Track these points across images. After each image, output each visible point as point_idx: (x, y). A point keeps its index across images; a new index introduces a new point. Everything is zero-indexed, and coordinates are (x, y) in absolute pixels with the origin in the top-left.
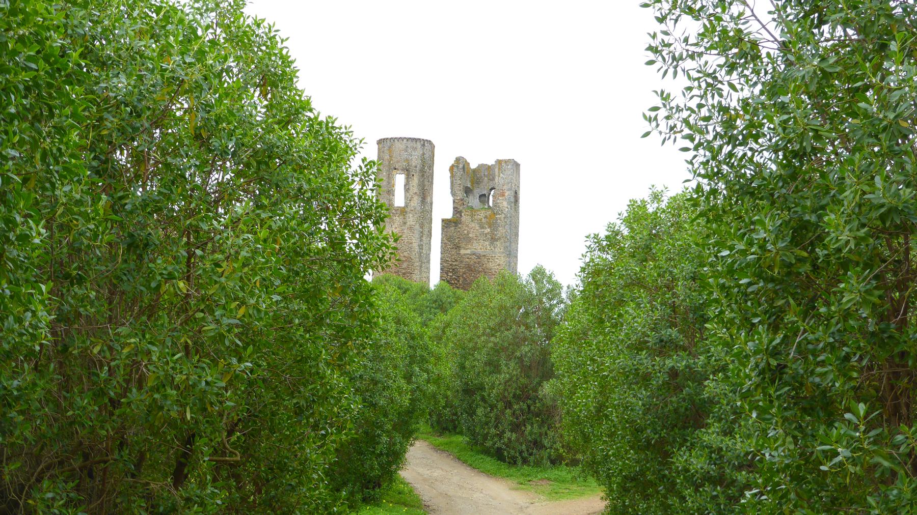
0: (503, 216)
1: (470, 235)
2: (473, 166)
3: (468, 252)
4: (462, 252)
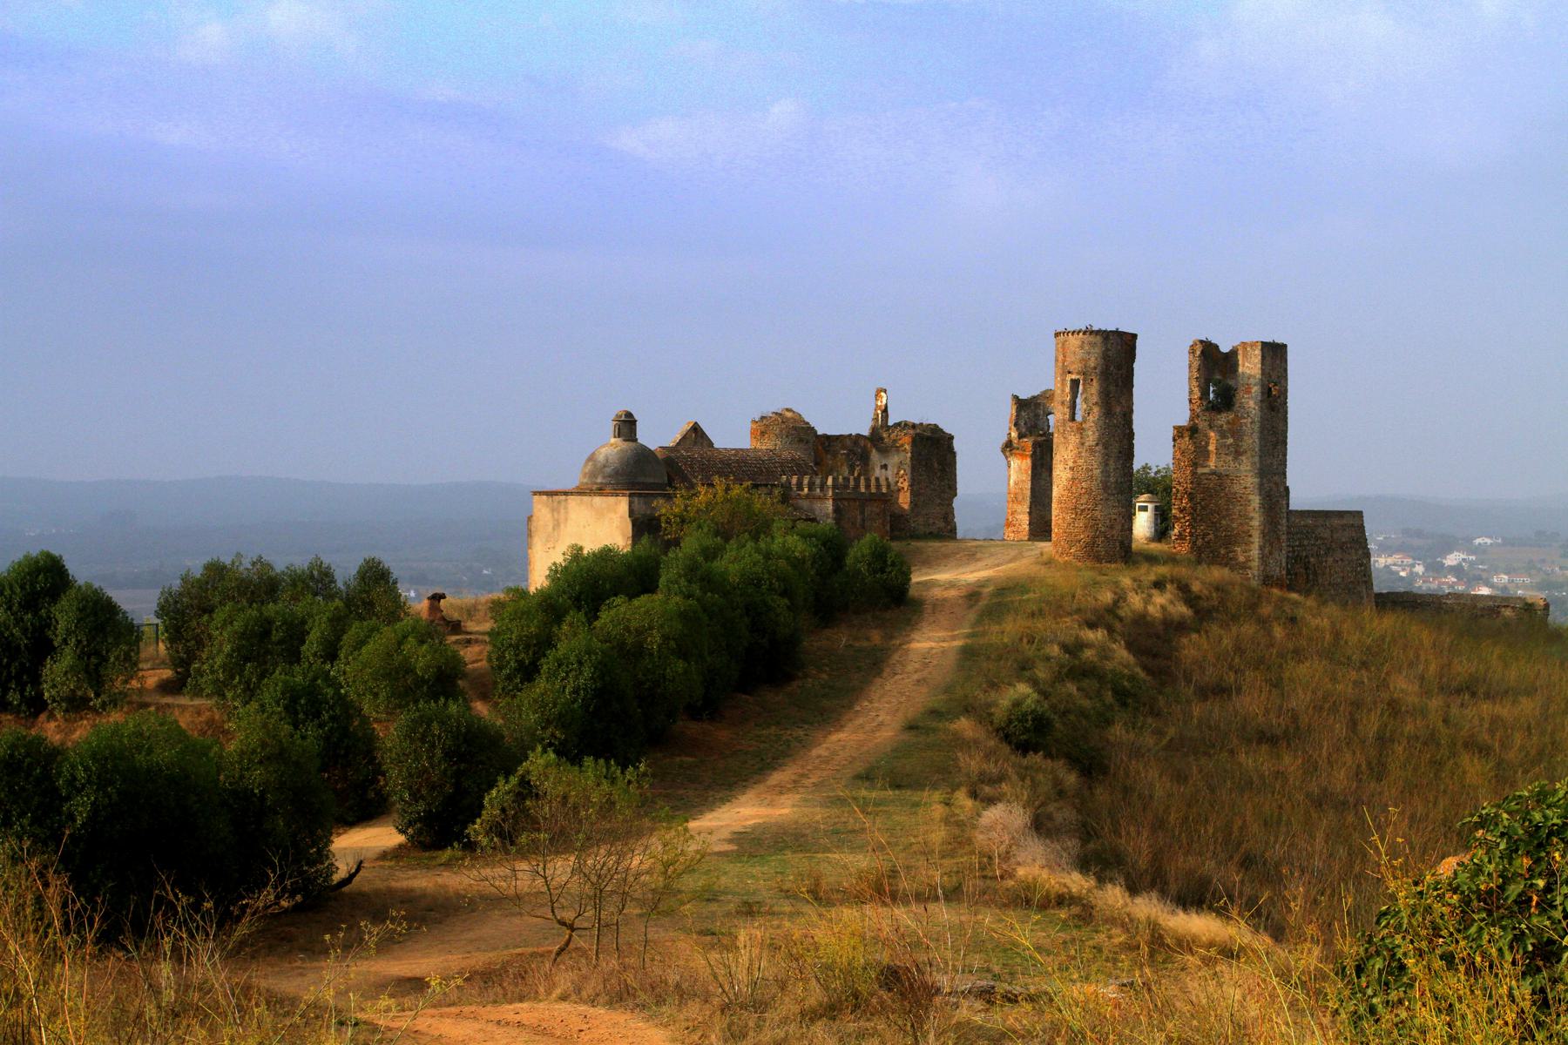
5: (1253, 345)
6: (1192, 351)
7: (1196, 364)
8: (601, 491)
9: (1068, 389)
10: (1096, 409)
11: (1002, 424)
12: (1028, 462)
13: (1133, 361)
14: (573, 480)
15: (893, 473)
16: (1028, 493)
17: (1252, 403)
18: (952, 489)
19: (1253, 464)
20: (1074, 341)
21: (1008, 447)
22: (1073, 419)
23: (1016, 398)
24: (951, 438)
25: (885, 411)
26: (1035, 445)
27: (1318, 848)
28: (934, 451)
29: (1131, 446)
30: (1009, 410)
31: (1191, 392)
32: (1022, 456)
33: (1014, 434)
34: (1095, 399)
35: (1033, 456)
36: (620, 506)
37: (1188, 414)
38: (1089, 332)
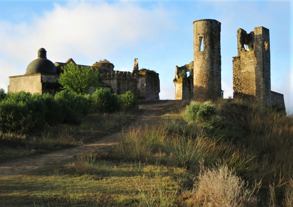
0: (259, 53)
1: (245, 63)
2: (248, 32)
3: (244, 71)
4: (242, 71)
5: (259, 28)
6: (238, 31)
7: (240, 36)
8: (32, 74)
9: (198, 40)
10: (208, 47)
11: (173, 74)
12: (181, 84)
13: (220, 32)
14: (24, 72)
15: (142, 83)
16: (182, 94)
17: (259, 47)
18: (158, 90)
19: (261, 67)
20: (200, 23)
21: (175, 80)
22: (200, 50)
23: (177, 66)
24: (158, 74)
25: (138, 65)
26: (183, 79)
27: (70, 184)
28: (153, 78)
29: (220, 61)
30: (175, 70)
31: (238, 45)
32: (180, 83)
33: (177, 77)
34: (208, 43)
35: (183, 82)
36: (38, 78)
37: (237, 53)
38: (206, 20)
